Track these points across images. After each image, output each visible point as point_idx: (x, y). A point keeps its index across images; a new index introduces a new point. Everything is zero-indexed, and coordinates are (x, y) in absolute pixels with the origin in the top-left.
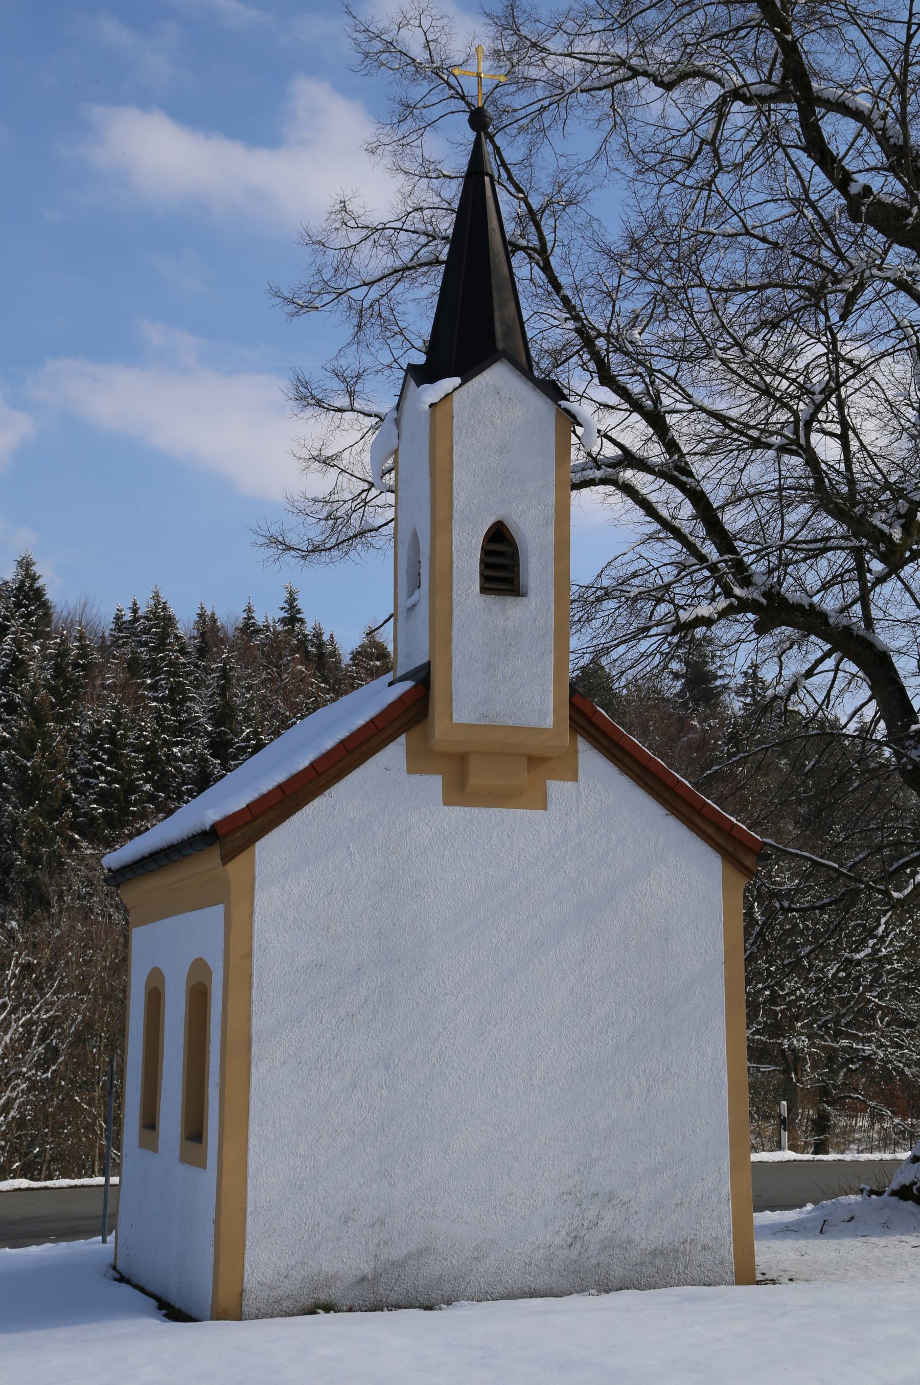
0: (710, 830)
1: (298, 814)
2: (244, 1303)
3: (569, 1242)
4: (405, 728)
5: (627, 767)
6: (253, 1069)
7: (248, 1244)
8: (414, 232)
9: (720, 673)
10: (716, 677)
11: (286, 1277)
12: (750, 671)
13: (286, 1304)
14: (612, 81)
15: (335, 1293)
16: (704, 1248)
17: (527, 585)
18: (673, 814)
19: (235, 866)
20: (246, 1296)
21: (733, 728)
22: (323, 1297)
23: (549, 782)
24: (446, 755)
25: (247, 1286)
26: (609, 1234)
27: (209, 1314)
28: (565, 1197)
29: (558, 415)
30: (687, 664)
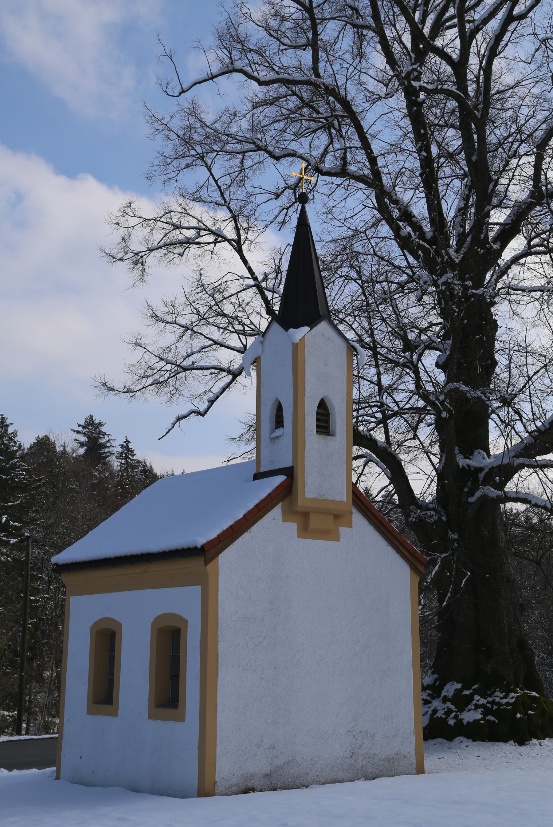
0: (406, 553)
1: (237, 541)
2: (216, 788)
3: (350, 755)
4: (281, 500)
5: (372, 520)
6: (219, 670)
7: (217, 758)
8: (166, 223)
9: (108, 444)
10: (106, 447)
11: (233, 775)
12: (125, 444)
13: (234, 789)
14: (245, 150)
15: (256, 783)
16: (405, 757)
17: (335, 431)
18: (391, 545)
19: (210, 567)
20: (217, 785)
21: (121, 478)
22: (249, 784)
23: (296, 524)
24: (298, 513)
25: (217, 779)
26: (367, 751)
27: (196, 795)
28: (349, 733)
29: (348, 347)
30: (89, 437)
